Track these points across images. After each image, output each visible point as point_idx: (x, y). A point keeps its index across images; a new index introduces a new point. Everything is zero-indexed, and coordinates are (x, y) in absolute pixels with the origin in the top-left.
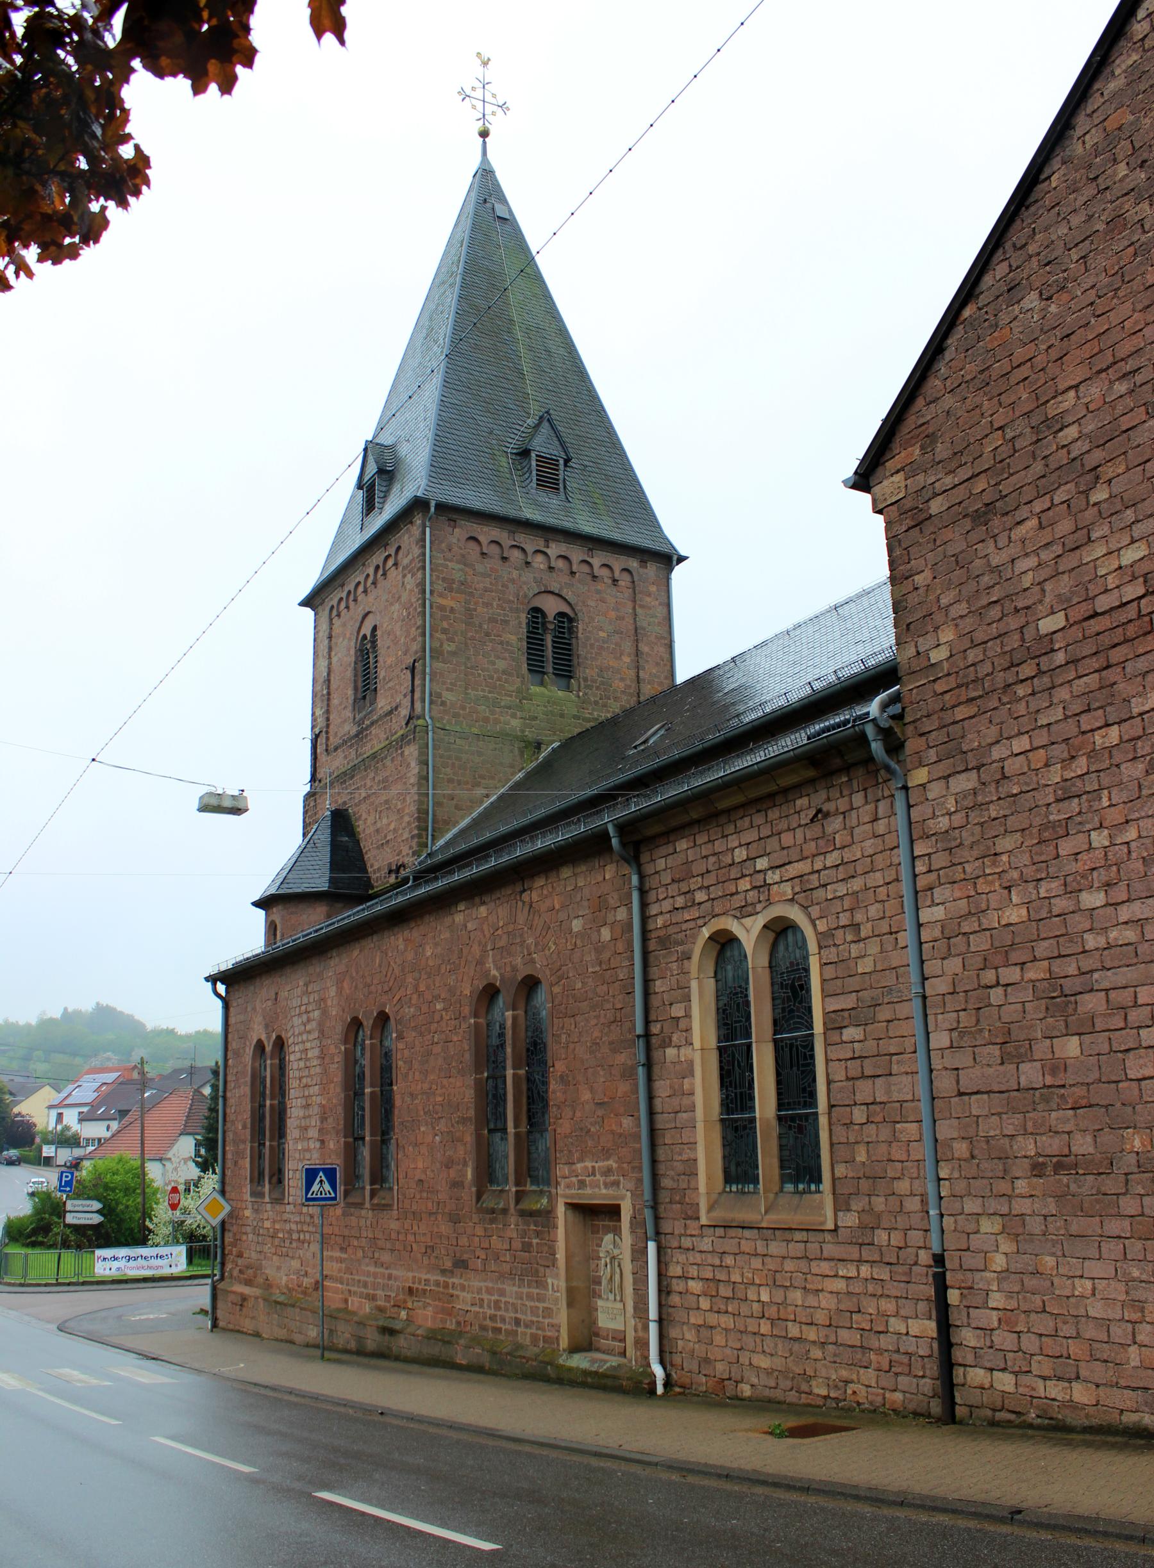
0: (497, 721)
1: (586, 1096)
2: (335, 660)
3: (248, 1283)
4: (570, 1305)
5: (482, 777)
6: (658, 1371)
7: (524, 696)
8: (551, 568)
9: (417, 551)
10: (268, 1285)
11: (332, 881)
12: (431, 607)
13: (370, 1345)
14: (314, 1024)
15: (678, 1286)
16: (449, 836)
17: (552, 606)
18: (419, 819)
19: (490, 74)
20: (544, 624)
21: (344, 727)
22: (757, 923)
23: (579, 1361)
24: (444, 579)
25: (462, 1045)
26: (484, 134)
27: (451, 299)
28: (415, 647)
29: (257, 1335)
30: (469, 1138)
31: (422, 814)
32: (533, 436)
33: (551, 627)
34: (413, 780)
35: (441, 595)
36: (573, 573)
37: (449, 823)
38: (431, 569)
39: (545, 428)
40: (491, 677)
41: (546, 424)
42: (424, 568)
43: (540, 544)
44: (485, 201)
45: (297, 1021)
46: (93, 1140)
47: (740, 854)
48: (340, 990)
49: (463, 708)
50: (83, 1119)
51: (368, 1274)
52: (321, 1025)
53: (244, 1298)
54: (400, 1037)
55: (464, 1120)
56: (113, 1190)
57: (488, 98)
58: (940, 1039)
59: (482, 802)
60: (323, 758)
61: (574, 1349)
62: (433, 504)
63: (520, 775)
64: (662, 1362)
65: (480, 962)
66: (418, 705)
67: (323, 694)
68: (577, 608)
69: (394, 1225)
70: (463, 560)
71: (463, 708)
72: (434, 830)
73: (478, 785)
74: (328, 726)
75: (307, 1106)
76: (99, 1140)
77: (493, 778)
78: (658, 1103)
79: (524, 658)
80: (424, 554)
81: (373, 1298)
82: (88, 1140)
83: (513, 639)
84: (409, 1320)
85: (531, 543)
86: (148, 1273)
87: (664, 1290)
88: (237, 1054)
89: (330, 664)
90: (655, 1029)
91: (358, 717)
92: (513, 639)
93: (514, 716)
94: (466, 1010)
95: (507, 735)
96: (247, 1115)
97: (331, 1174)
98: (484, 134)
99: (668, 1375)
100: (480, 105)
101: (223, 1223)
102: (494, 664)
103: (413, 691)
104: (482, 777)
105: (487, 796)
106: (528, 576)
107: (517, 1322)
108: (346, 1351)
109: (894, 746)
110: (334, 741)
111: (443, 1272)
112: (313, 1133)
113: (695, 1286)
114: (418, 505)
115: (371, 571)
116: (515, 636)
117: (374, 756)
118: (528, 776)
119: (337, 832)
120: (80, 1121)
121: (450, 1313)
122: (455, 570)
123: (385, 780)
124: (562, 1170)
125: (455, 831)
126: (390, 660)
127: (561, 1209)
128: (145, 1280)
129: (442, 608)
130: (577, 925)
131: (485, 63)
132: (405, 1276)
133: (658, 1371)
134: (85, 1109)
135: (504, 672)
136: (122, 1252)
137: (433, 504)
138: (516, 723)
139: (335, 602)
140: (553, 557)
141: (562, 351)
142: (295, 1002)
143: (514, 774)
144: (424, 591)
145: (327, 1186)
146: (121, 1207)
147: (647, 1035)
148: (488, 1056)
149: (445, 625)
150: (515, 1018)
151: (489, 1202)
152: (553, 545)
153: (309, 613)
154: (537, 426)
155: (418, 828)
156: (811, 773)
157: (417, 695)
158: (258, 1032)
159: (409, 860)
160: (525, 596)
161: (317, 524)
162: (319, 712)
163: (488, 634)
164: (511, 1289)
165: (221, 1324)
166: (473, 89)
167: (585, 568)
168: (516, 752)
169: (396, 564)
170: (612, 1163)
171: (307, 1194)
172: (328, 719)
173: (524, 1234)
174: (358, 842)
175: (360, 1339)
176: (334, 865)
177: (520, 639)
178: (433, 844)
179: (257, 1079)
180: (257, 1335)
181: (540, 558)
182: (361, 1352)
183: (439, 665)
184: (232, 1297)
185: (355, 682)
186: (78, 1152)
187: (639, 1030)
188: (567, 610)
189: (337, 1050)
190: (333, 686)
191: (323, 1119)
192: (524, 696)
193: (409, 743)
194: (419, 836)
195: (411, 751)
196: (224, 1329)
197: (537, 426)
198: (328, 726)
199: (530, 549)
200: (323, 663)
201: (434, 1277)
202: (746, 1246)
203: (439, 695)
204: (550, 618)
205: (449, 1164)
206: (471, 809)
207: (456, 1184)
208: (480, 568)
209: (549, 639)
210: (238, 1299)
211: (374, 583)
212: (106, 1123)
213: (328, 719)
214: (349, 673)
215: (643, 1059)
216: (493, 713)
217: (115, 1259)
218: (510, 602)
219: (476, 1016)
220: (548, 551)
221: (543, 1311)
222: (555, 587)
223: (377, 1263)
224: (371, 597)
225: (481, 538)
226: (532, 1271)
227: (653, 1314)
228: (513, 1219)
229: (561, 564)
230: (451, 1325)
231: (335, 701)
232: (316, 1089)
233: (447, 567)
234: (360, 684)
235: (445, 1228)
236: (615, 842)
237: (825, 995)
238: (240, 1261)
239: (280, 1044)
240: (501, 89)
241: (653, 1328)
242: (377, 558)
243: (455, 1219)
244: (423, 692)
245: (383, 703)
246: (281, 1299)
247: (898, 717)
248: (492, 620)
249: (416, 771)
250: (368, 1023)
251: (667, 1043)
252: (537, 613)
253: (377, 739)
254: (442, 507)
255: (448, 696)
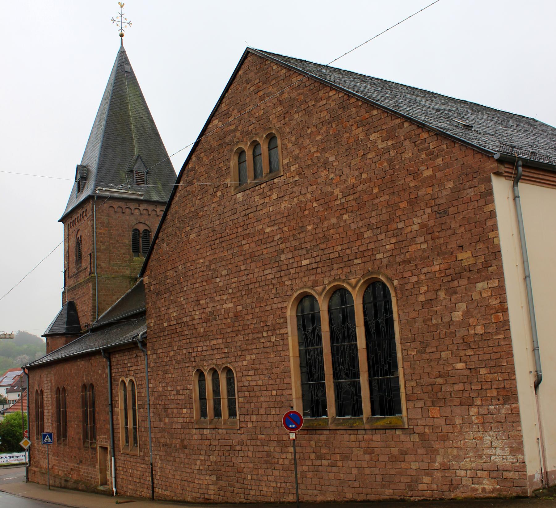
0: (121, 272)
1: (102, 418)
2: (70, 244)
3: (37, 467)
4: (100, 473)
5: (116, 292)
6: (114, 490)
7: (131, 261)
8: (141, 214)
9: (91, 213)
10: (41, 468)
11: (67, 328)
12: (96, 233)
13: (63, 485)
14: (49, 388)
15: (118, 469)
16: (104, 314)
17: (142, 228)
18: (93, 309)
19: (124, 10)
20: (139, 234)
21: (73, 271)
22: (128, 379)
23: (101, 488)
24: (101, 223)
25: (80, 400)
26: (122, 36)
27: (107, 107)
28: (91, 248)
29: (38, 483)
30: (81, 427)
31: (94, 307)
32: (135, 164)
33: (141, 235)
34: (91, 295)
35: (100, 229)
36: (149, 215)
37: (105, 309)
38: (96, 220)
39: (139, 162)
40: (119, 256)
41: (139, 159)
42: (93, 220)
43: (137, 205)
44: (121, 65)
45: (45, 385)
46: (13, 401)
47: (126, 362)
48: (55, 378)
49: (109, 268)
50: (8, 392)
51: (63, 464)
52: (51, 388)
53: (35, 472)
54: (68, 395)
55: (80, 422)
56: (14, 427)
57: (124, 20)
58: (152, 415)
59: (116, 301)
60: (67, 279)
61: (102, 484)
62: (96, 197)
63: (129, 290)
64: (116, 487)
65: (83, 377)
66: (92, 269)
67: (67, 257)
68: (151, 228)
69: (68, 450)
70: (108, 215)
71: (109, 268)
72: (98, 312)
73: (114, 295)
74: (69, 268)
75: (48, 412)
76: (15, 400)
77: (119, 292)
78: (114, 421)
79: (131, 248)
80: (93, 215)
81: (64, 471)
82: (10, 401)
83: (127, 241)
84: (72, 478)
85: (133, 206)
86: (18, 462)
87: (116, 470)
88: (32, 393)
89: (69, 245)
90: (113, 402)
91: (78, 267)
92: (127, 241)
93: (127, 269)
94: (80, 390)
95: (125, 276)
96: (34, 413)
97: (50, 435)
98: (122, 36)
99: (117, 491)
100: (120, 24)
101: (30, 447)
102: (120, 251)
103: (91, 264)
104: (116, 292)
105: (118, 299)
106: (133, 218)
107: (91, 477)
108: (58, 487)
109: (144, 344)
110: (71, 274)
111: (78, 464)
112: (50, 421)
113: (120, 468)
114: (90, 198)
115: (79, 215)
116: (128, 241)
117: (81, 284)
118: (132, 291)
119: (70, 308)
120: (7, 392)
121: (79, 475)
122: (105, 219)
123: (83, 293)
124: (98, 437)
125: (106, 312)
126: (86, 249)
127: (98, 448)
128: (17, 464)
129: (100, 233)
130: (100, 371)
131: (122, 6)
132: (71, 465)
133: (114, 490)
134: (9, 388)
135: (124, 254)
136: (8, 455)
137: (96, 197)
138: (128, 272)
139: (69, 223)
140: (142, 210)
141: (149, 126)
142: (45, 379)
143: (127, 290)
144: (93, 228)
145: (49, 439)
146: (18, 434)
147: (112, 404)
148: (84, 404)
149: (101, 239)
150: (89, 394)
151: (85, 445)
152: (141, 206)
153: (61, 224)
154: (136, 160)
155: (93, 312)
156: (134, 346)
157: (92, 265)
158: (36, 387)
159: (91, 323)
160: (132, 225)
161: (61, 194)
162: (66, 262)
163: (117, 241)
164: (90, 468)
165: (30, 480)
166: (117, 17)
167: (154, 213)
168: (128, 282)
169: (86, 215)
170: (106, 436)
171: (44, 440)
172: (68, 265)
173: (92, 454)
174: (77, 313)
175: (61, 483)
176: (68, 323)
177: (130, 241)
178: (98, 317)
179: (37, 401)
180: (38, 483)
181: (137, 211)
182: (61, 487)
183: (98, 254)
184: (32, 472)
185: (76, 254)
186: (6, 406)
187: (110, 403)
188: (148, 228)
189: (55, 396)
190: (70, 254)
191: (52, 417)
192: (131, 261)
193: (90, 282)
194: (93, 315)
195: (90, 285)
196: (31, 482)
197: (136, 160)
198: (69, 268)
199: (133, 208)
200: (67, 245)
201: (76, 465)
202: (360, 437)
203: (100, 265)
204: (141, 231)
205: (78, 433)
206: (112, 304)
207: (79, 439)
208: (114, 217)
209: (141, 240)
210: (33, 472)
211: (80, 220)
212: (18, 393)
213: (68, 265)
214: (74, 250)
215: (110, 410)
216: (119, 269)
217: (5, 457)
218: (126, 228)
219: (82, 392)
220: (140, 208)
221: (93, 474)
222: (143, 221)
223: (65, 461)
224: (80, 224)
225: (114, 206)
226: (93, 465)
227: (113, 475)
228: (90, 450)
229: (145, 212)
230: (79, 479)
231: (71, 259)
232: (50, 408)
233: (101, 218)
234: (78, 255)
235: (78, 452)
236: (102, 353)
237: (138, 400)
238: (34, 460)
239: (42, 391)
240: (129, 17)
241: (113, 479)
242: (80, 211)
243: (80, 449)
244: (94, 264)
245: (84, 264)
246: (44, 472)
247: (146, 337)
248: (119, 235)
249: (92, 292)
250: (61, 390)
251: (115, 407)
252: (136, 231)
253: (81, 279)
254: (99, 197)
255: (103, 265)
